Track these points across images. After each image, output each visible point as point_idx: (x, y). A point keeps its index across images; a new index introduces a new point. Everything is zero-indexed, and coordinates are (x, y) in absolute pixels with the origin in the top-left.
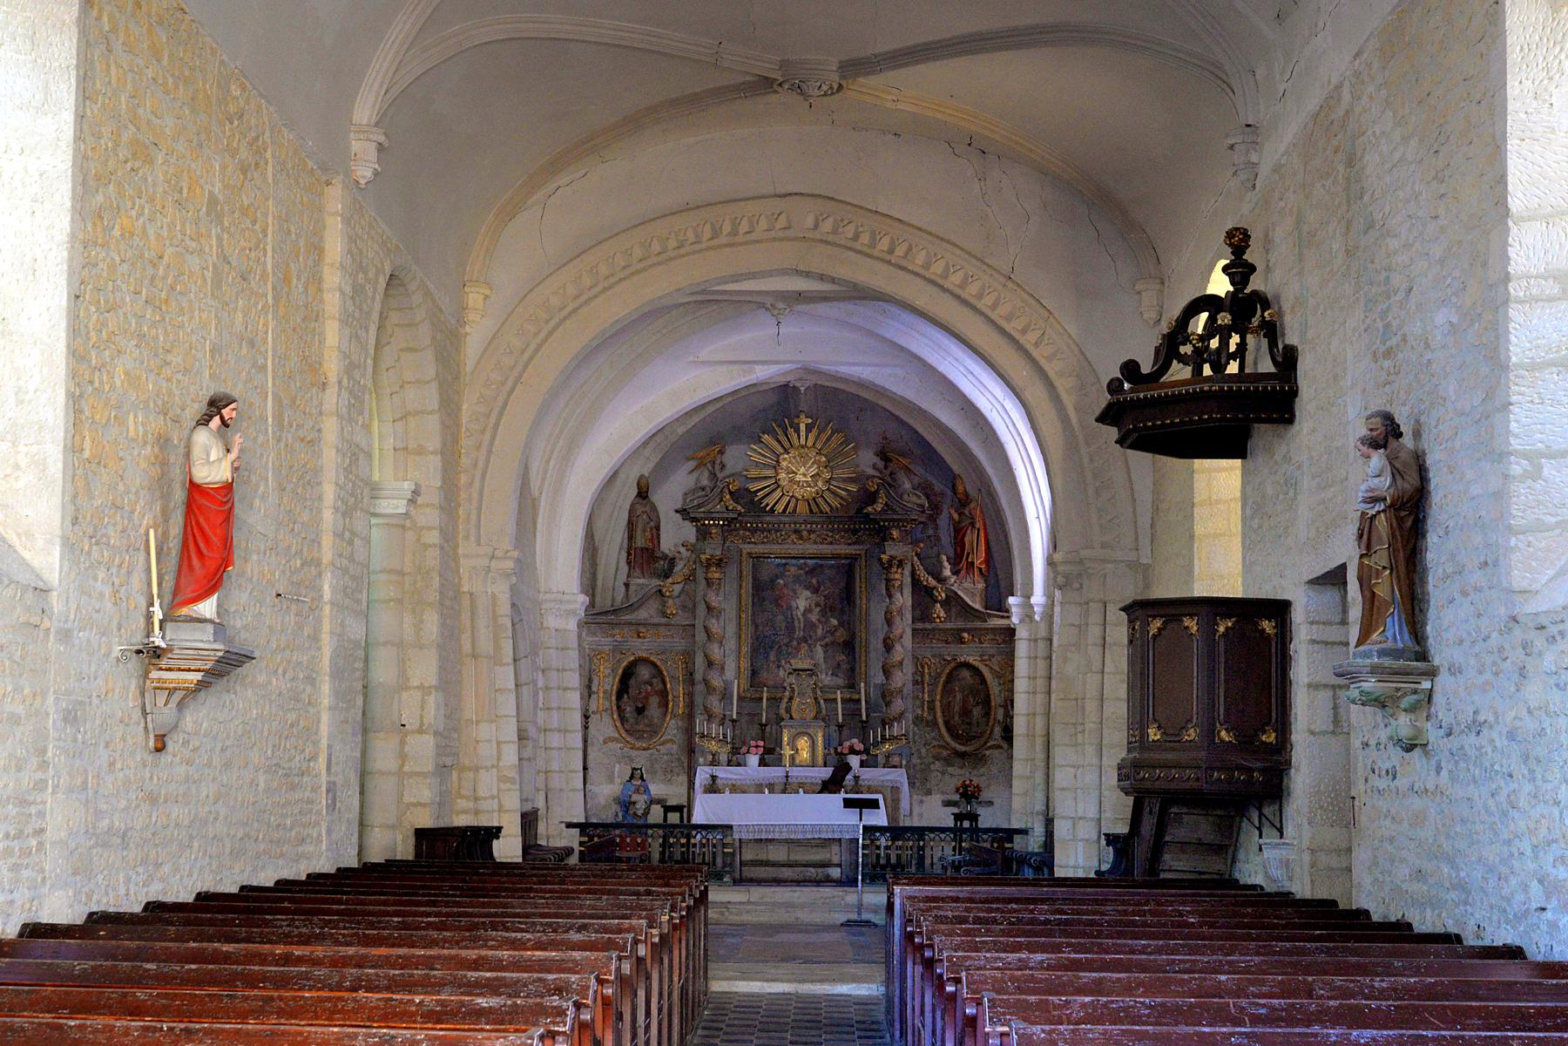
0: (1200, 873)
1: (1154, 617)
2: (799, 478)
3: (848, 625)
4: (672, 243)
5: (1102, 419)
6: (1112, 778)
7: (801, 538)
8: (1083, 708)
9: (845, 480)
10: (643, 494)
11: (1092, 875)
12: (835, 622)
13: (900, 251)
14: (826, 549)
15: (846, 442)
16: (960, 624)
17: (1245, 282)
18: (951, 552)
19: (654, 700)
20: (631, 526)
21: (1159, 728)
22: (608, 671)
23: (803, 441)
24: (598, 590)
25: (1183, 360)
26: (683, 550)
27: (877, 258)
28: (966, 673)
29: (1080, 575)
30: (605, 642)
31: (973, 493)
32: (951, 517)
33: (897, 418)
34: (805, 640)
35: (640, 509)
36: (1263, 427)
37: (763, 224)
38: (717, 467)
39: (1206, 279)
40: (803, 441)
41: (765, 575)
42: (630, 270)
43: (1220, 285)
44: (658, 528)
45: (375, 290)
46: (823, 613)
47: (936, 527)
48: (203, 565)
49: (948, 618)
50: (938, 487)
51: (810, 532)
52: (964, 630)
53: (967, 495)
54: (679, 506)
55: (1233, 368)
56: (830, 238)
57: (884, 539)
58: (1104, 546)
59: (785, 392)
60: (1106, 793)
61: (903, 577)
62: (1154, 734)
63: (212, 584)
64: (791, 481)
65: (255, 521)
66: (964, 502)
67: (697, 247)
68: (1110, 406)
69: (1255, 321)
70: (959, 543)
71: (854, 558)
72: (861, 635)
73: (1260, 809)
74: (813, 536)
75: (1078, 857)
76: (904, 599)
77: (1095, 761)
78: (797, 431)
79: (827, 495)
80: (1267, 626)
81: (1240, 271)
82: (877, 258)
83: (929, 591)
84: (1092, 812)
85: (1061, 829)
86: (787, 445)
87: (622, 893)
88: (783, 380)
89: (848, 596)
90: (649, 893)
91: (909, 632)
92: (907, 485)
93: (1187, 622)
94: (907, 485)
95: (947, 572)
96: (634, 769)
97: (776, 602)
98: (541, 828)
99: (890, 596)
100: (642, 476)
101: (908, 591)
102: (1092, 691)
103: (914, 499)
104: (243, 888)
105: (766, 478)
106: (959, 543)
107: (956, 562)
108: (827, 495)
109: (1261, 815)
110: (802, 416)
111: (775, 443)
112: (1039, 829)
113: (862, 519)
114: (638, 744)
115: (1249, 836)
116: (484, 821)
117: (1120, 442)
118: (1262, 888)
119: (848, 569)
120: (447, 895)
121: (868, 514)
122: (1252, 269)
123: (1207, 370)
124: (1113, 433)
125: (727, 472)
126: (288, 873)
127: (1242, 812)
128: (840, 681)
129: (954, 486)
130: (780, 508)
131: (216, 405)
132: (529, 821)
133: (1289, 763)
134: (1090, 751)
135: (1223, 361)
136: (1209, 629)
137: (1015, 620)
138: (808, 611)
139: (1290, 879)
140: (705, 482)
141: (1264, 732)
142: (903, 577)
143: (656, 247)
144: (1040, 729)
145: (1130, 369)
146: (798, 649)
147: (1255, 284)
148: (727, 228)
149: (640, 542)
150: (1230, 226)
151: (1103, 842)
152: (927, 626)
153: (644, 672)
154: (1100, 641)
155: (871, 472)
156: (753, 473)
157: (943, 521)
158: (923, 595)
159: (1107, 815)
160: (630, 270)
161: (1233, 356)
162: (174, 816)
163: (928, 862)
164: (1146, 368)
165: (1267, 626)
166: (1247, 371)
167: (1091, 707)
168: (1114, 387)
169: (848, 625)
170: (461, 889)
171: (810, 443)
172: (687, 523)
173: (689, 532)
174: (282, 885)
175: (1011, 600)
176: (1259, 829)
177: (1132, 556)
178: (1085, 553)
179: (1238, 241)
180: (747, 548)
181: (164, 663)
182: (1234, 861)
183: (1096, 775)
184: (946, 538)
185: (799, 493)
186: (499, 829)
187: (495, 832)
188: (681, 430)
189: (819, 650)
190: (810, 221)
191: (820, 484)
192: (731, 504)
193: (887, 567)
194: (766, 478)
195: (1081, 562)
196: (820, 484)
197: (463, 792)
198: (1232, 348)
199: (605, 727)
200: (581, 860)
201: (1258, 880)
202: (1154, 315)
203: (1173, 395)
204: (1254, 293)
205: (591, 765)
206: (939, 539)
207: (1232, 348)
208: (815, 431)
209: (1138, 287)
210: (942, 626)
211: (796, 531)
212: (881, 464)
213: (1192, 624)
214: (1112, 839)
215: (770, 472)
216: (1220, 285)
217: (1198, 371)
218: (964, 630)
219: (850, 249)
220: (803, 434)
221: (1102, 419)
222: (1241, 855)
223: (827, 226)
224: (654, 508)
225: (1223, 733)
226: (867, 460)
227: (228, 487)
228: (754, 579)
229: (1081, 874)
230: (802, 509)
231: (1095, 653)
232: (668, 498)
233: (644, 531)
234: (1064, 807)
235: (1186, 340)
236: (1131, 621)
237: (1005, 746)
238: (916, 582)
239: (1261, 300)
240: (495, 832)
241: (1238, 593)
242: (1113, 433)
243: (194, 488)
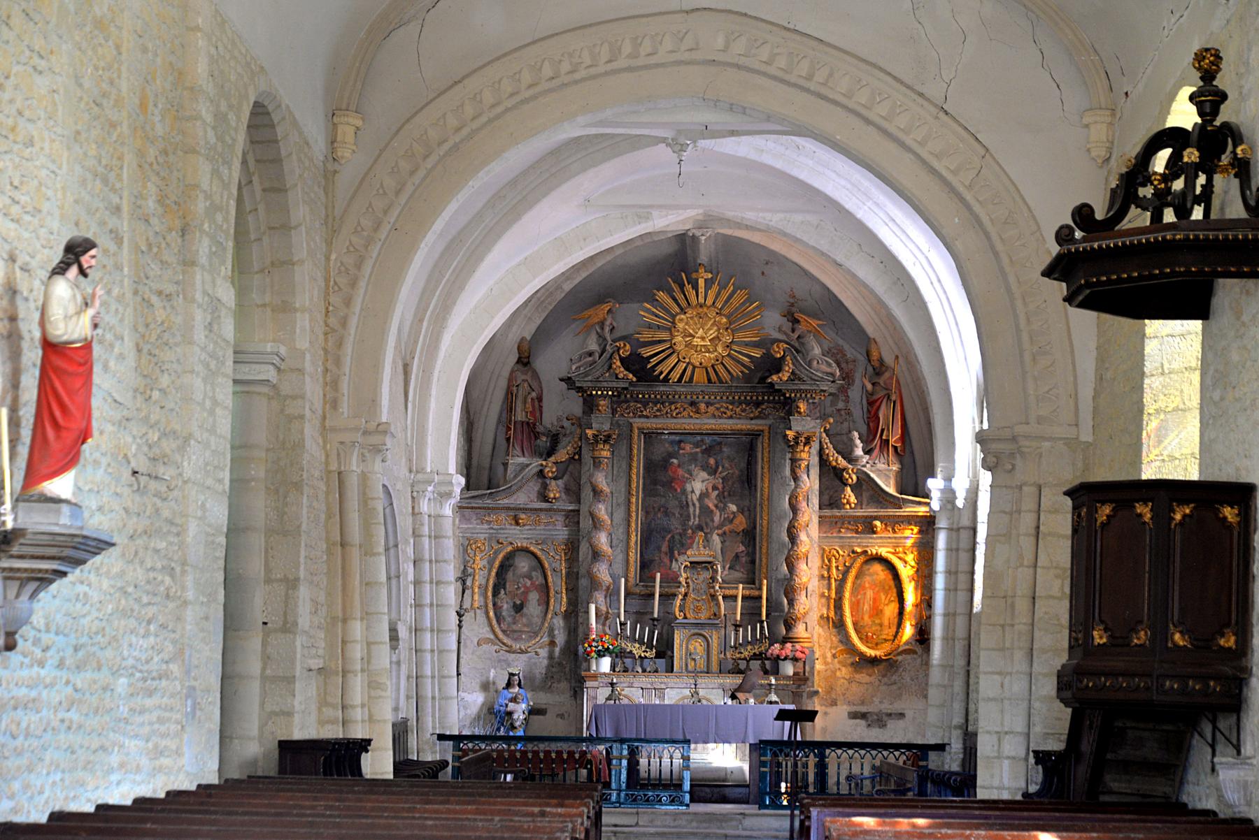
0: (1144, 796)
1: (1103, 503)
2: (697, 341)
3: (750, 512)
4: (565, 67)
5: (1048, 273)
6: (1049, 687)
7: (697, 412)
8: (1013, 606)
9: (747, 344)
10: (524, 361)
11: (1019, 797)
12: (733, 508)
13: (820, 76)
14: (726, 424)
15: (750, 301)
16: (871, 511)
17: (1215, 112)
18: (864, 429)
19: (534, 597)
20: (510, 397)
21: (1106, 630)
22: (485, 562)
23: (701, 300)
24: (473, 471)
25: (1142, 204)
26: (567, 424)
27: (795, 85)
28: (877, 568)
29: (1012, 455)
30: (481, 530)
31: (889, 359)
32: (864, 386)
33: (805, 272)
34: (700, 528)
35: (520, 377)
36: (1221, 281)
37: (668, 44)
38: (607, 329)
39: (1166, 111)
40: (701, 300)
41: (660, 450)
42: (518, 98)
43: (1184, 115)
44: (540, 399)
45: (239, 118)
46: (721, 497)
47: (847, 401)
48: (58, 437)
49: (860, 504)
50: (850, 352)
51: (708, 404)
52: (876, 518)
53: (881, 361)
54: (564, 374)
55: (1198, 213)
56: (742, 61)
57: (790, 413)
58: (1040, 420)
59: (684, 242)
60: (1036, 705)
61: (809, 456)
62: (1099, 638)
63: (69, 460)
64: (688, 345)
65: (108, 386)
66: (879, 369)
67: (593, 71)
68: (1059, 258)
69: (1225, 159)
70: (872, 418)
71: (755, 435)
72: (762, 523)
73: (1214, 722)
74: (711, 409)
75: (1003, 775)
76: (811, 482)
77: (1024, 667)
78: (696, 287)
79: (727, 361)
80: (1229, 513)
81: (1209, 100)
82: (795, 85)
83: (838, 473)
84: (1020, 727)
85: (985, 746)
86: (684, 303)
87: (516, 814)
88: (681, 228)
89: (749, 480)
90: (543, 814)
91: (815, 520)
92: (817, 351)
93: (1140, 508)
94: (817, 351)
95: (859, 451)
96: (512, 675)
97: (669, 484)
98: (413, 742)
99: (796, 478)
100: (523, 339)
101: (815, 472)
102: (1023, 589)
103: (824, 368)
104: (99, 807)
105: (660, 342)
106: (872, 418)
107: (867, 442)
108: (727, 361)
109: (1215, 728)
110: (701, 270)
111: (670, 301)
112: (956, 746)
113: (765, 387)
114: (516, 646)
115: (1200, 752)
116: (358, 733)
117: (1069, 299)
118: (1215, 813)
119: (749, 445)
120: (323, 816)
121: (772, 385)
122: (1223, 97)
123: (1169, 216)
124: (1062, 288)
125: (617, 334)
126: (146, 791)
127: (1193, 725)
128: (737, 575)
129: (868, 354)
130: (675, 376)
131: (75, 252)
132: (400, 733)
133: (1248, 671)
134: (1019, 655)
135: (1189, 205)
136: (1163, 516)
137: (936, 505)
138: (703, 495)
139: (1249, 804)
140: (593, 346)
141: (1223, 635)
142: (809, 456)
143: (547, 71)
144: (960, 632)
145: (1083, 214)
146: (692, 538)
147: (1226, 114)
148: (627, 49)
149: (520, 416)
150: (1196, 47)
151: (1032, 760)
152: (836, 512)
153: (523, 564)
154: (1033, 531)
155: (776, 335)
156: (646, 336)
157: (855, 393)
158: (832, 477)
159: (1037, 729)
160: (518, 98)
161: (1197, 200)
162: (24, 725)
163: (832, 780)
164: (1099, 215)
165: (1229, 513)
166: (1213, 216)
167: (1022, 605)
168: (1063, 236)
169: (750, 512)
170: (338, 808)
171: (709, 302)
172: (573, 392)
173: (575, 405)
174: (140, 803)
175: (931, 483)
176: (1213, 747)
177: (1071, 433)
178: (1020, 429)
179: (1208, 65)
180: (638, 422)
181: (15, 550)
182: (1182, 783)
183: (1025, 684)
184: (858, 412)
185: (696, 358)
186: (369, 741)
187: (364, 745)
188: (568, 287)
189: (716, 539)
190: (720, 42)
191: (720, 349)
192: (622, 372)
193: (792, 446)
194: (660, 342)
195: (1014, 439)
196: (720, 349)
197: (329, 699)
198: (1198, 190)
199: (477, 627)
200: (453, 777)
201: (1210, 804)
202: (1103, 153)
203: (1207, 239)
204: (1226, 125)
205: (462, 671)
206: (849, 413)
207: (1198, 190)
208: (715, 288)
209: (1086, 120)
210: (851, 513)
211: (693, 404)
212: (787, 326)
213: (1145, 511)
214: (1041, 757)
215: (664, 335)
216: (1184, 115)
217: (1157, 217)
218: (876, 518)
219: (765, 74)
220: (701, 290)
221: (1048, 273)
222: (1191, 776)
223: (739, 47)
224: (536, 376)
225: (1177, 636)
226: (772, 322)
227: (88, 346)
228: (646, 458)
229: (1006, 796)
230: (699, 376)
231: (1027, 543)
232: (555, 362)
233: (525, 402)
234: (988, 722)
235: (1147, 180)
236: (1075, 508)
237: (919, 649)
238: (823, 461)
239: (1231, 133)
240: (364, 745)
241: (1192, 473)
242: (1062, 288)
243: (50, 347)
